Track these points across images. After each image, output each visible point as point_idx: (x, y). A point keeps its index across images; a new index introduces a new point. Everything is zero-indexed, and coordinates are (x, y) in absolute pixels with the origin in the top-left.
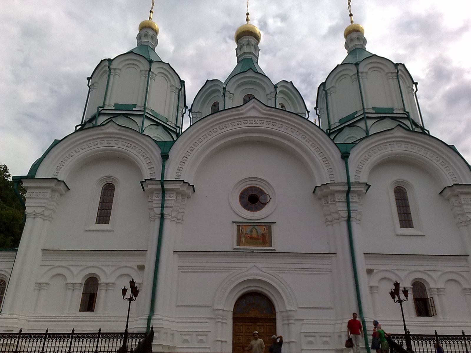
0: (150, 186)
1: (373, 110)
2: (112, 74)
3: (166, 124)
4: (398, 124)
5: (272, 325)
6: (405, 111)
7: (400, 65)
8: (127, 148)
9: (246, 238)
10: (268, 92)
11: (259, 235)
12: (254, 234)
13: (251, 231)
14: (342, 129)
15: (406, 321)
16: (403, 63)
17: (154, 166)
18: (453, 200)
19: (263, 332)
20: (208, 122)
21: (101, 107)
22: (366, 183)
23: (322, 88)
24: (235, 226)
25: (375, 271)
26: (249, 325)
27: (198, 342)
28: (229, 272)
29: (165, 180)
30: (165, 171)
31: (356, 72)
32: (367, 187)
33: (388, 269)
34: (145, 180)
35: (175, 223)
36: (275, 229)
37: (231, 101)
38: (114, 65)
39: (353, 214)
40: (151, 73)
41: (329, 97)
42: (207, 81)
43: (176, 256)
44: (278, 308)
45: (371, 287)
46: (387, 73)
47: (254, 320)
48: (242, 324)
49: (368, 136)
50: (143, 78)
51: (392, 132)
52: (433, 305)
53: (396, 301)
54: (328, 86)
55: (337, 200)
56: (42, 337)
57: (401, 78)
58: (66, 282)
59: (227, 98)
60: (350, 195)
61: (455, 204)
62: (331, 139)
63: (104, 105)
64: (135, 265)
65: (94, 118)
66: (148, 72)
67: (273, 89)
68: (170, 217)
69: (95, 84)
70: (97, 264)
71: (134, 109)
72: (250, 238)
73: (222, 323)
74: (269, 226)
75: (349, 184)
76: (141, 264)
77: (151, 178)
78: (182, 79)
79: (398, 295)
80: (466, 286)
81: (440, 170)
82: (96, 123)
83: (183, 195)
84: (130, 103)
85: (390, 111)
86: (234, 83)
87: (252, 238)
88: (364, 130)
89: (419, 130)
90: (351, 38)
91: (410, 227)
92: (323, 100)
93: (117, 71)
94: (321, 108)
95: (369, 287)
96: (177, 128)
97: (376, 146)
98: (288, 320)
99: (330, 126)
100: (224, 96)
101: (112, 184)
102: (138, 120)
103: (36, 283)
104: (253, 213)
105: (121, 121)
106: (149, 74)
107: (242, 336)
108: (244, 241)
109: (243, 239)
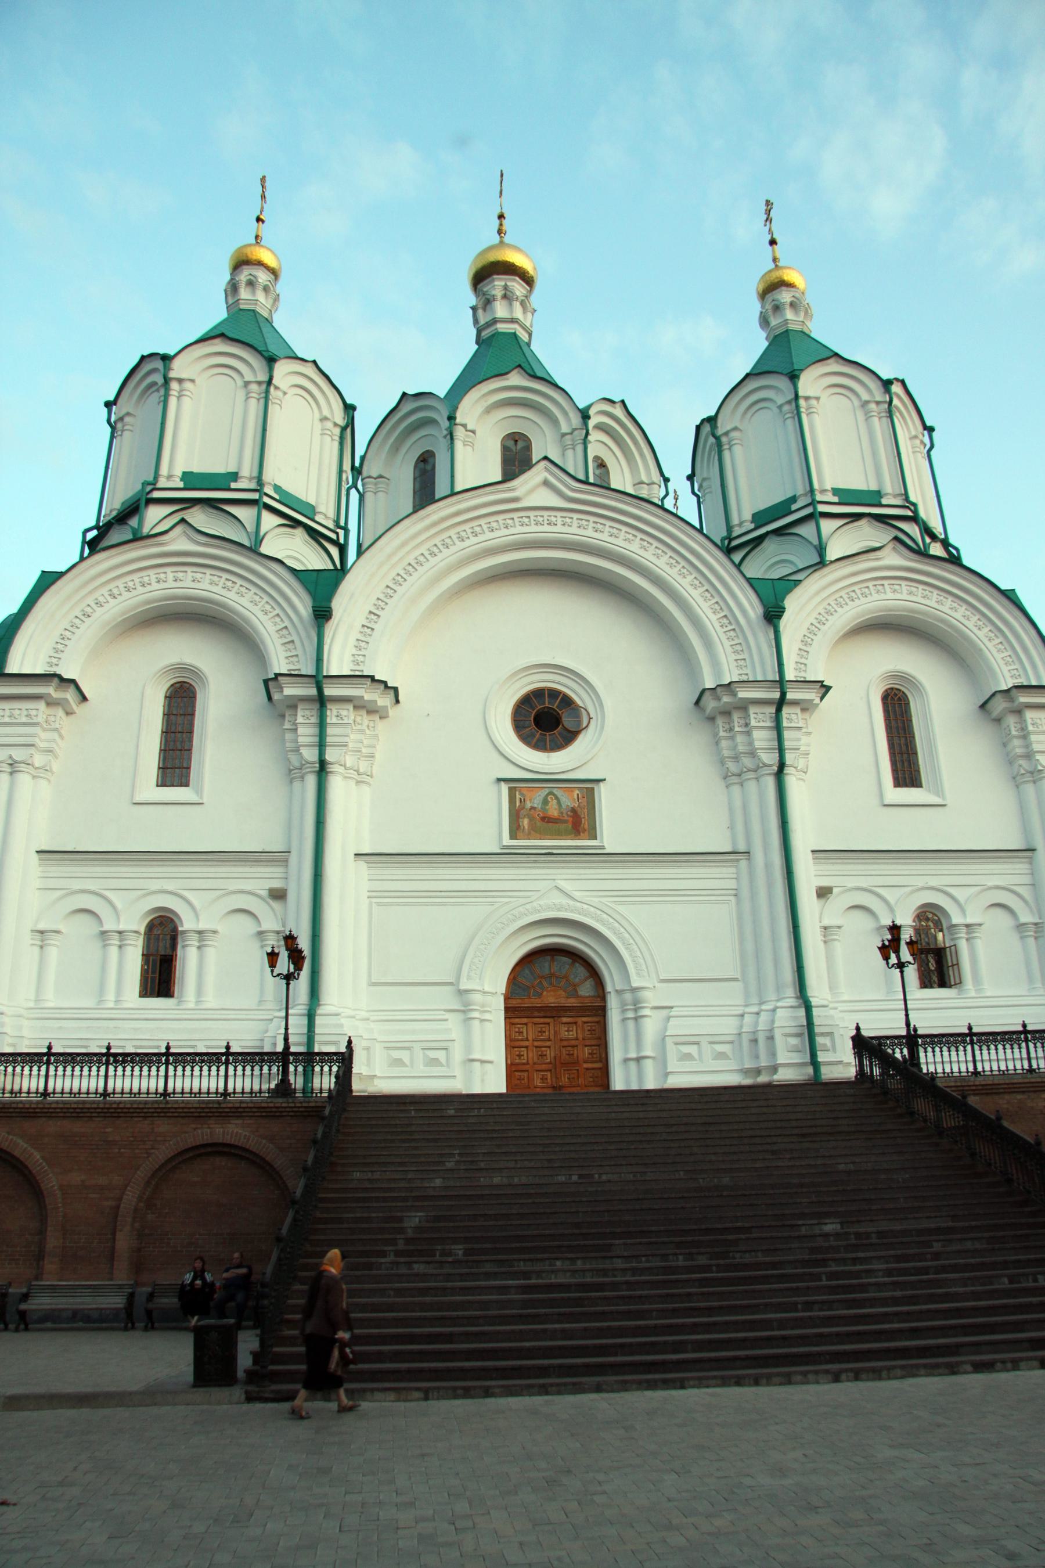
0: (288, 691)
1: (834, 495)
2: (172, 393)
3: (313, 520)
4: (891, 538)
5: (597, 1022)
6: (907, 499)
7: (895, 382)
8: (224, 592)
9: (531, 819)
10: (565, 428)
11: (565, 812)
12: (553, 811)
13: (545, 802)
14: (760, 539)
15: (900, 1000)
16: (901, 378)
17: (295, 637)
18: (1011, 721)
19: (577, 1039)
20: (427, 522)
21: (149, 484)
22: (823, 681)
23: (706, 429)
24: (505, 788)
25: (835, 890)
26: (545, 1024)
27: (426, 1065)
28: (491, 904)
29: (325, 674)
30: (326, 648)
31: (793, 396)
32: (823, 690)
33: (864, 885)
34: (275, 674)
35: (352, 783)
36: (604, 796)
37: (469, 449)
38: (178, 369)
39: (789, 758)
40: (272, 389)
41: (726, 454)
42: (404, 394)
43: (362, 864)
44: (612, 983)
45: (825, 928)
46: (867, 402)
47: (554, 1012)
48: (525, 1020)
49: (822, 563)
50: (876, 420)
51: (878, 554)
52: (955, 963)
53: (890, 966)
54: (723, 426)
55: (753, 723)
56: (41, 1061)
57: (898, 414)
58: (101, 929)
59: (459, 445)
60: (785, 710)
61: (1014, 733)
62: (733, 562)
63: (157, 476)
64: (262, 887)
65: (131, 511)
66: (264, 386)
67: (576, 420)
68: (341, 769)
69: (127, 419)
70: (170, 886)
71: (233, 485)
72: (543, 819)
73: (482, 1021)
74: (588, 788)
75: (781, 683)
76: (277, 884)
77: (289, 670)
78: (348, 402)
79: (897, 952)
80: (1026, 917)
81: (987, 651)
82: (141, 523)
83: (372, 710)
84: (220, 469)
85: (874, 498)
86: (477, 401)
87: (546, 819)
88: (815, 547)
89: (936, 550)
90: (776, 302)
91: (917, 786)
92: (709, 454)
93: (188, 385)
94: (704, 479)
95: (821, 927)
96: (338, 530)
97: (843, 588)
98: (636, 1010)
99: (729, 528)
100: (452, 439)
101: (188, 683)
102: (243, 513)
103: (32, 931)
104: (548, 757)
105: (198, 517)
106: (267, 392)
107: (527, 1047)
108: (526, 827)
109: (525, 822)
